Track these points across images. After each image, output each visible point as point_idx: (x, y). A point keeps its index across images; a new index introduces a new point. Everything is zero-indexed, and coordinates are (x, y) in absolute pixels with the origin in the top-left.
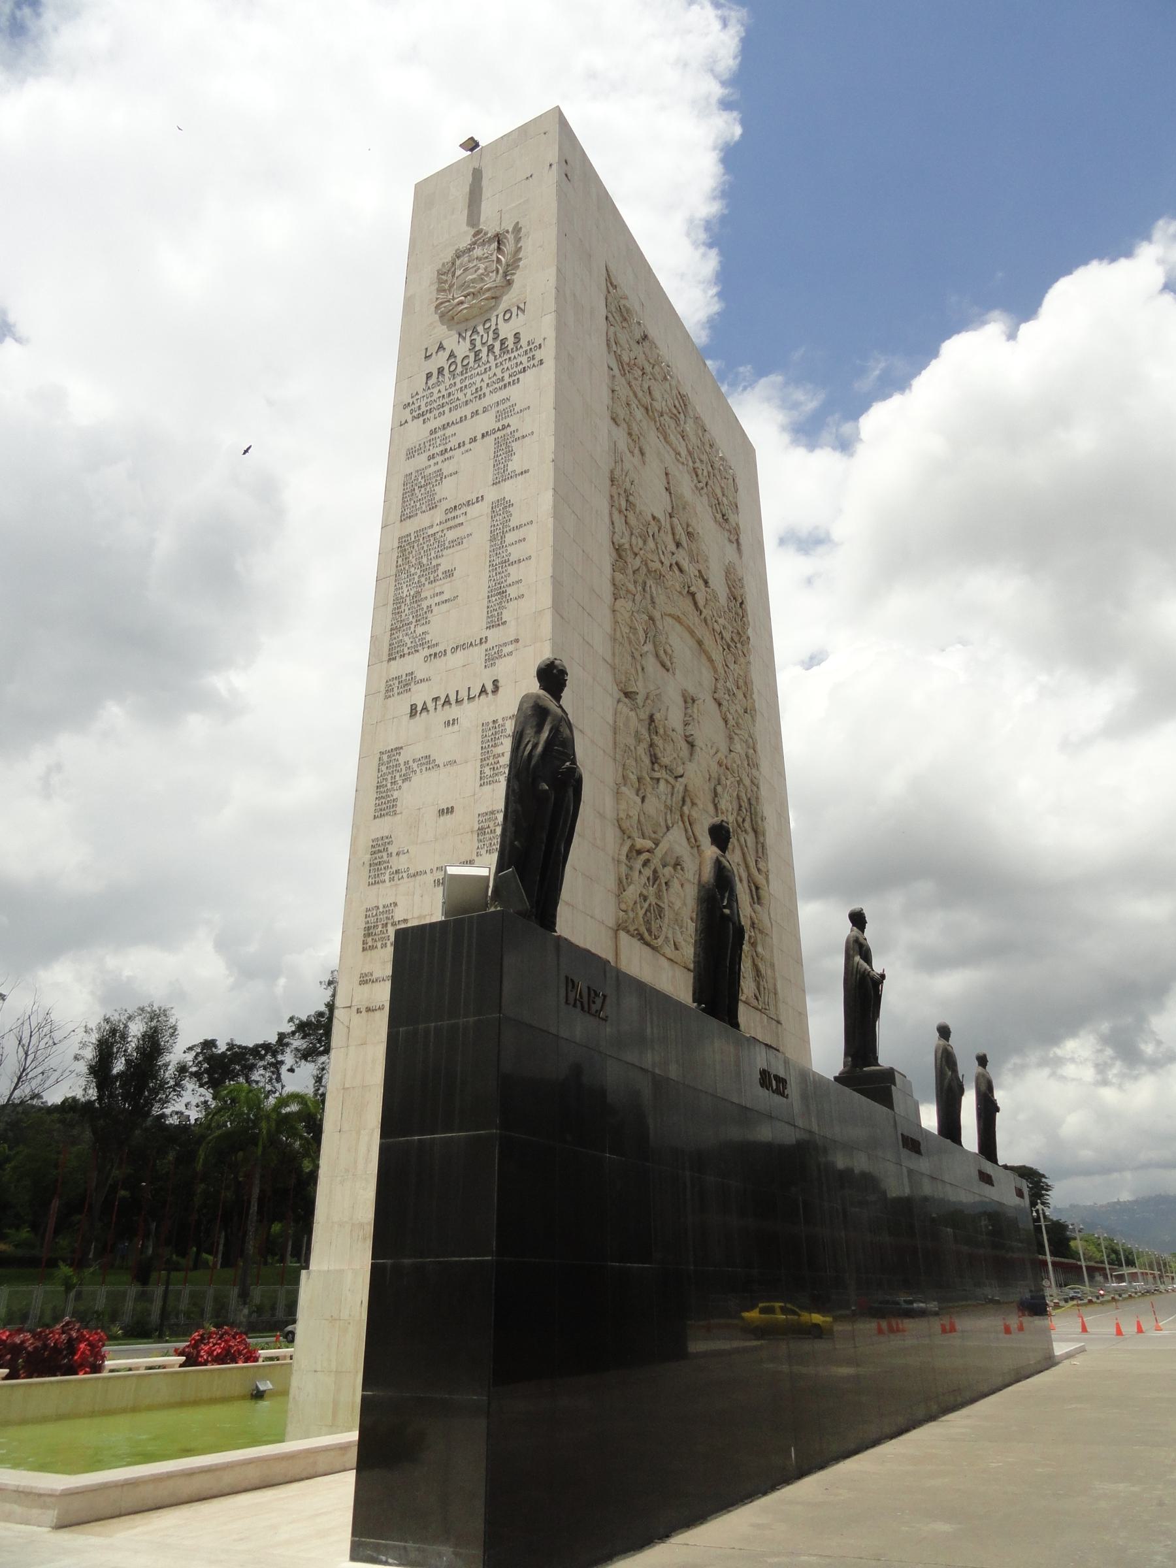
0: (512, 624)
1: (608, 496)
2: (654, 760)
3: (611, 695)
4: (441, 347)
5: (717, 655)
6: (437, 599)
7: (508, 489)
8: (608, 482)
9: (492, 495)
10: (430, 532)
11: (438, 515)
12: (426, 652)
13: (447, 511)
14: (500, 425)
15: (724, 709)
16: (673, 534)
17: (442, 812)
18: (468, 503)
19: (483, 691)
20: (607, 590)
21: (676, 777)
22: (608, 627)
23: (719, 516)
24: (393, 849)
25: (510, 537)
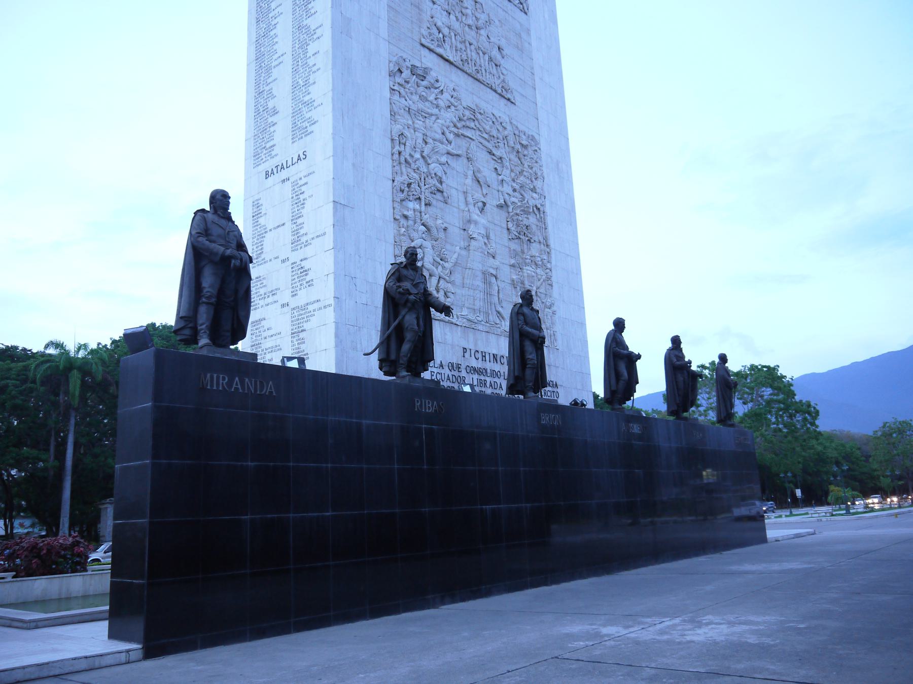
5: (472, 125)
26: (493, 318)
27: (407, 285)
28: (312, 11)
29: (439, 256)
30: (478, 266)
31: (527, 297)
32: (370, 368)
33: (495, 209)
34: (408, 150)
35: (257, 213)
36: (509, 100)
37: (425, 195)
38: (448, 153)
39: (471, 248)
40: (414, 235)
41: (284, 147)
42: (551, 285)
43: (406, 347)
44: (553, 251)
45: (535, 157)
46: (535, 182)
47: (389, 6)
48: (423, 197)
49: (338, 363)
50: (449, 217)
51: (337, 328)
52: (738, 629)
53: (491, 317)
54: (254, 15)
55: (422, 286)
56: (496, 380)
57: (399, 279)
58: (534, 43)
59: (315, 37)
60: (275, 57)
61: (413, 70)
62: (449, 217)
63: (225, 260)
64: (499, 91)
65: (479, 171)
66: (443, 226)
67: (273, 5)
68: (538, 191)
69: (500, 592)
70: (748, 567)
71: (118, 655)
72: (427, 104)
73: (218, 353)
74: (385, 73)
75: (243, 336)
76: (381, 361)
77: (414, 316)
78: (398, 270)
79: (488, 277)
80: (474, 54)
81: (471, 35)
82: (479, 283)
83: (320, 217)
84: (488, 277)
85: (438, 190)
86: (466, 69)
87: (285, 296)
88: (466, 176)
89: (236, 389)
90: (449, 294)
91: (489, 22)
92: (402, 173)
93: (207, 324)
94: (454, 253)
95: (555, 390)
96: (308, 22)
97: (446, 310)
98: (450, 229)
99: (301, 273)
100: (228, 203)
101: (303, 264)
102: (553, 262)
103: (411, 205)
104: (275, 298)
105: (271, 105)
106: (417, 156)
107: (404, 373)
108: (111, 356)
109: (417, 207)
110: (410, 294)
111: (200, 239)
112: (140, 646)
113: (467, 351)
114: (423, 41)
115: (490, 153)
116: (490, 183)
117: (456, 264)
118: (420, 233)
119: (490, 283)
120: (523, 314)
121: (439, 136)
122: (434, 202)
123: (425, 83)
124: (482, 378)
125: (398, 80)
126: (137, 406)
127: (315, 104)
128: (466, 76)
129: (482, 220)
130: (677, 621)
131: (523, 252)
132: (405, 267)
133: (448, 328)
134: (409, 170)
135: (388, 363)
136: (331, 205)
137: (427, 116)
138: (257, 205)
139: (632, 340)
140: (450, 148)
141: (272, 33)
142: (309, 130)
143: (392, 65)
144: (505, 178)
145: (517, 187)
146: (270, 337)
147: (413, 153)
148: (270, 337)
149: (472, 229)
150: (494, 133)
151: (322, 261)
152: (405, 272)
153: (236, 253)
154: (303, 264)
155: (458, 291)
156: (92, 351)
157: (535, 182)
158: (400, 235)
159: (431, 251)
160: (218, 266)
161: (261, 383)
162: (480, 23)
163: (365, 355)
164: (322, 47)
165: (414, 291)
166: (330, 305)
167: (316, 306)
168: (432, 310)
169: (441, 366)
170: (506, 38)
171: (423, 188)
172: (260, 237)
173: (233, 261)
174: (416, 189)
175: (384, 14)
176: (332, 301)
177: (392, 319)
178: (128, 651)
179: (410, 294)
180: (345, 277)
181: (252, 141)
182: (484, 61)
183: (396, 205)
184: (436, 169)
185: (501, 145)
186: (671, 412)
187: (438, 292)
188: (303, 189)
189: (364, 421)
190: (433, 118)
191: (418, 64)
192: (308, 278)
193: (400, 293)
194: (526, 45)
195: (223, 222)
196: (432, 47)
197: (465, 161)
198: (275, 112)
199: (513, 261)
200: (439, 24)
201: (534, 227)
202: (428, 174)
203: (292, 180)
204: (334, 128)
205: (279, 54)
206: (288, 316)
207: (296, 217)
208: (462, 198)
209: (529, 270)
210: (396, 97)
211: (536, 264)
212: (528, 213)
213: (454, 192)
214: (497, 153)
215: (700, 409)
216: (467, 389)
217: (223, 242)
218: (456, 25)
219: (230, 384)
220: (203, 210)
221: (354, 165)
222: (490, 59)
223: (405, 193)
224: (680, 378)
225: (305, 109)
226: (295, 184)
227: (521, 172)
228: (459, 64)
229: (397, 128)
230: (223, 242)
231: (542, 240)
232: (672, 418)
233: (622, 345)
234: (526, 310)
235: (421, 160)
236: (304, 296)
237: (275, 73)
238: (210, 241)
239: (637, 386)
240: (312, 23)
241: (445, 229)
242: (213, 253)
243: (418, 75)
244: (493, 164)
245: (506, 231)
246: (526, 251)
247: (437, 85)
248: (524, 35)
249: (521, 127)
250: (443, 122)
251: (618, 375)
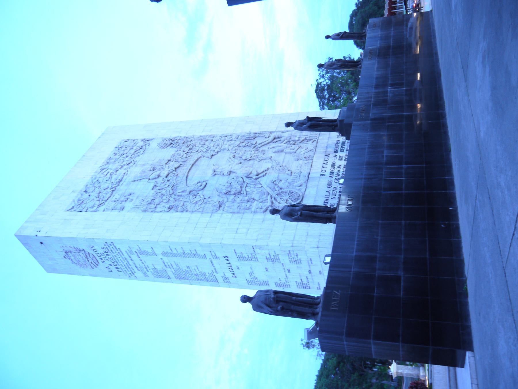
0: (205, 252)
1: (152, 213)
2: (240, 193)
3: (222, 214)
4: (108, 267)
5: (195, 156)
6: (197, 270)
7: (158, 251)
8: (147, 213)
9: (161, 256)
10: (174, 272)
11: (168, 270)
12: (215, 273)
13: (167, 267)
14: (135, 254)
15: (214, 153)
16: (156, 178)
17: (267, 270)
18: (164, 262)
19: (227, 260)
20: (186, 215)
21: (244, 182)
22: (199, 215)
23: (142, 151)
24: (279, 282)
25: (175, 252)
126: (347, 345)
148: (312, 280)
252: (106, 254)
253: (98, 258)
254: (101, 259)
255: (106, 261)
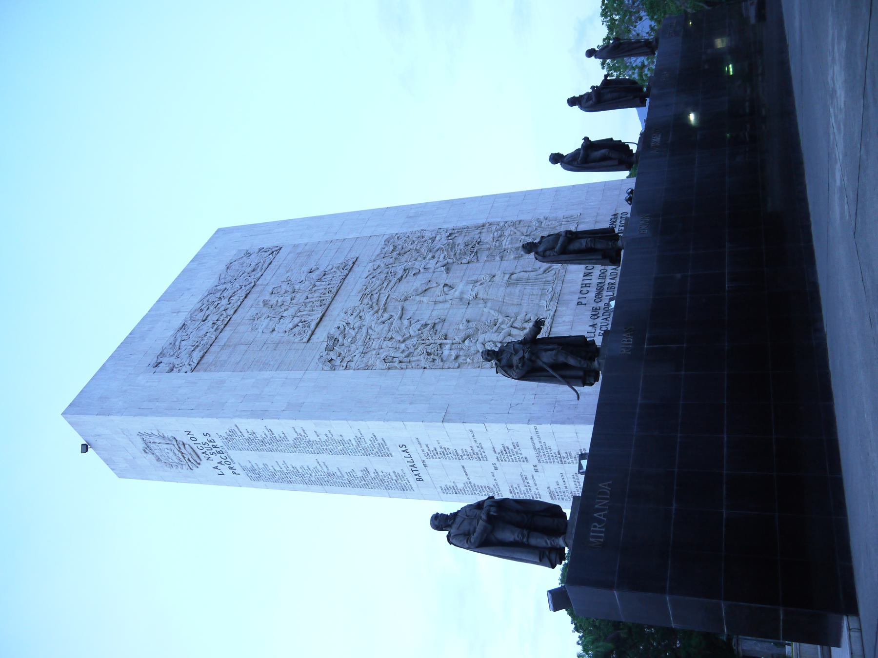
4: (216, 468)
5: (376, 296)
19: (406, 451)
26: (550, 276)
27: (515, 360)
28: (282, 435)
29: (492, 327)
30: (501, 291)
31: (529, 248)
32: (591, 394)
33: (450, 275)
34: (398, 354)
35: (451, 490)
36: (354, 263)
37: (437, 339)
38: (401, 318)
39: (485, 297)
40: (473, 349)
41: (396, 463)
42: (520, 221)
43: (572, 361)
44: (490, 220)
45: (404, 238)
46: (426, 238)
47: (277, 369)
48: (439, 342)
49: (586, 422)
50: (457, 317)
51: (556, 422)
52: (837, 55)
53: (550, 279)
54: (285, 485)
55: (517, 346)
56: (608, 274)
57: (510, 366)
58: (306, 241)
59: (303, 434)
60: (320, 469)
61: (330, 349)
62: (457, 317)
63: (490, 519)
64: (347, 272)
65: (416, 290)
66: (465, 323)
67: (278, 469)
68: (433, 235)
69: (814, 273)
70: (797, 24)
71: (853, 639)
72: (358, 337)
73: (572, 530)
74: (332, 374)
75: (557, 508)
76: (584, 384)
77: (544, 354)
78: (502, 368)
79: (511, 282)
80: (315, 295)
81: (300, 298)
82: (517, 290)
83: (456, 435)
84: (511, 282)
85: (433, 327)
86: (328, 302)
87: (528, 468)
88: (421, 302)
89: (604, 516)
90: (527, 318)
91: (289, 282)
92: (418, 360)
93: (546, 538)
94: (489, 313)
95: (619, 216)
96: (291, 439)
97: (539, 324)
98: (468, 317)
99: (506, 453)
100: (442, 515)
101: (498, 451)
102: (499, 220)
103: (446, 352)
104: (529, 477)
105: (360, 474)
106: (403, 346)
107: (596, 364)
108: (590, 633)
109: (448, 347)
110: (524, 357)
111: (472, 540)
112: (845, 618)
113: (577, 304)
114: (305, 340)
115: (400, 280)
116: (427, 280)
117: (500, 312)
118: (471, 344)
119: (517, 280)
120: (545, 251)
121: (386, 327)
122: (444, 331)
123: (341, 339)
124: (606, 287)
125: (338, 362)
126: (618, 603)
127: (359, 435)
128: (334, 302)
129: (460, 287)
130: (832, 110)
131: (489, 249)
132: (499, 360)
133: (558, 320)
134: (415, 353)
135: (587, 379)
136: (446, 424)
137: (368, 336)
138: (446, 490)
139: (570, 146)
140: (396, 317)
141: (300, 470)
142: (380, 441)
143: (325, 368)
144: (423, 266)
145: (430, 255)
146: (559, 483)
147: (401, 350)
148: (559, 483)
149: (468, 296)
150: (383, 276)
151: (495, 435)
152: (504, 361)
153: (484, 511)
154: (498, 451)
155: (524, 309)
156: (584, 650)
157: (426, 238)
158: (473, 363)
159: (488, 334)
160: (498, 527)
161: (600, 493)
162: (290, 289)
163: (578, 398)
164: (310, 428)
165: (521, 353)
166: (536, 428)
167: (536, 441)
168: (539, 337)
169: (594, 326)
170: (302, 266)
171: (431, 341)
172: (474, 488)
173: (492, 513)
174: (431, 348)
175: (283, 374)
176: (532, 426)
177: (545, 374)
178: (849, 629)
179: (524, 357)
180: (509, 414)
181: (391, 491)
182: (321, 286)
183: (446, 366)
184: (415, 329)
185: (393, 270)
186: (642, 104)
187: (525, 328)
188: (431, 448)
189: (639, 402)
190: (370, 331)
191: (325, 344)
192: (511, 447)
193: (523, 366)
194: (307, 248)
195: (458, 520)
196: (310, 332)
197: (407, 302)
198: (366, 470)
199: (498, 258)
200: (291, 326)
201: (467, 239)
202: (419, 336)
203: (424, 459)
204: (379, 419)
205: (316, 464)
206: (545, 465)
207: (457, 456)
208: (440, 306)
209: (506, 243)
210: (352, 364)
211: (500, 236)
212: (454, 245)
213: (435, 313)
214: (400, 273)
215: (646, 63)
216: (613, 303)
217: (475, 521)
218: (292, 311)
219: (599, 521)
220: (448, 537)
221: (411, 403)
222: (319, 280)
223: (435, 357)
224: (609, 96)
225: (363, 445)
226: (427, 455)
227: (417, 251)
228: (324, 308)
229: (379, 364)
230: (475, 521)
231: (478, 231)
232: (648, 100)
233: (575, 155)
234: (541, 249)
235: (406, 343)
236: (528, 452)
237: (333, 469)
238: (474, 532)
239: (615, 139)
240: (291, 436)
241: (468, 321)
242: (485, 530)
243: (334, 345)
244: (410, 277)
245: (470, 265)
246: (488, 246)
247: (342, 328)
248: (299, 250)
249: (378, 252)
250: (373, 323)
251: (604, 158)
252: (211, 444)
253: (199, 452)
254: (204, 453)
255: (212, 457)
